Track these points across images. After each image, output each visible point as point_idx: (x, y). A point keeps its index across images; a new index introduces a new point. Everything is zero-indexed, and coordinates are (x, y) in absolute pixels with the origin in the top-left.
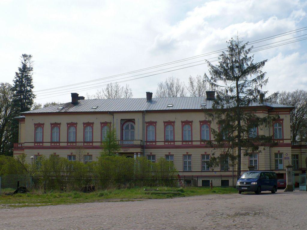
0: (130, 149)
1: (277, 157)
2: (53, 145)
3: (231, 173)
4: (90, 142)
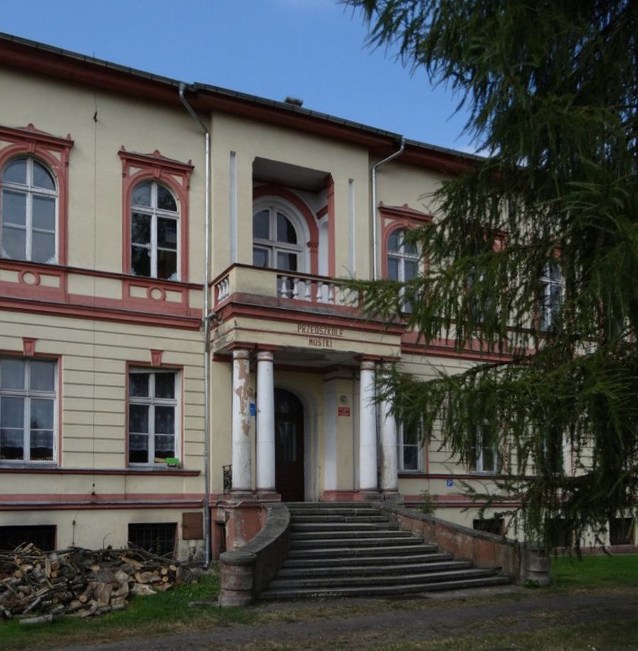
0: (347, 334)
1: (145, 394)
2: (50, 290)
4: (40, 267)
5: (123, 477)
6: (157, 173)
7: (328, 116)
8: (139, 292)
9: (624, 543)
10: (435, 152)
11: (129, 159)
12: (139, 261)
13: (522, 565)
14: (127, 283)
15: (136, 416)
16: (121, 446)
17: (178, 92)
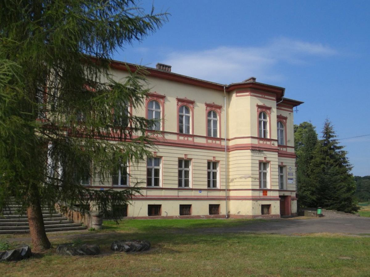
2: (181, 140)
3: (222, 194)
5: (177, 190)
6: (155, 99)
7: (152, 68)
8: (181, 138)
9: (186, 215)
10: (187, 78)
11: (179, 100)
12: (181, 130)
13: (90, 222)
14: (178, 135)
15: (180, 173)
16: (177, 182)
17: (224, 88)
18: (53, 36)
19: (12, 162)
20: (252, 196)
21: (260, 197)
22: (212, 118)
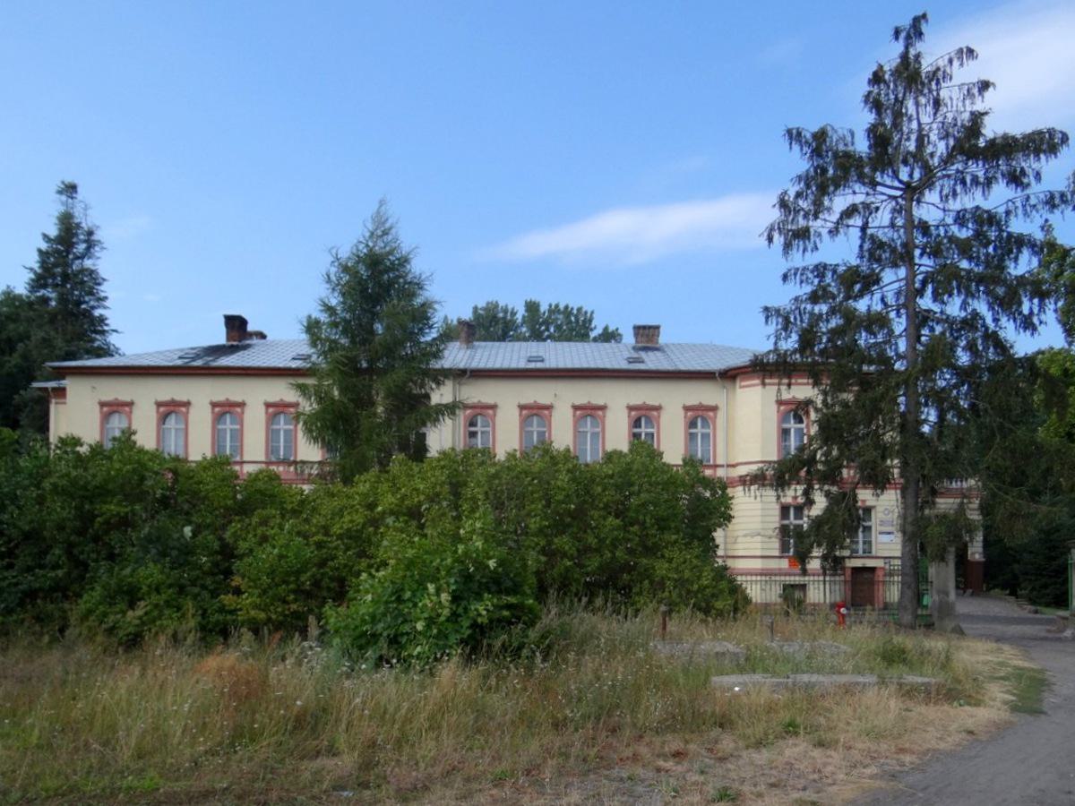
18: (162, 782)
19: (343, 353)
20: (762, 569)
21: (780, 569)
22: (699, 430)
